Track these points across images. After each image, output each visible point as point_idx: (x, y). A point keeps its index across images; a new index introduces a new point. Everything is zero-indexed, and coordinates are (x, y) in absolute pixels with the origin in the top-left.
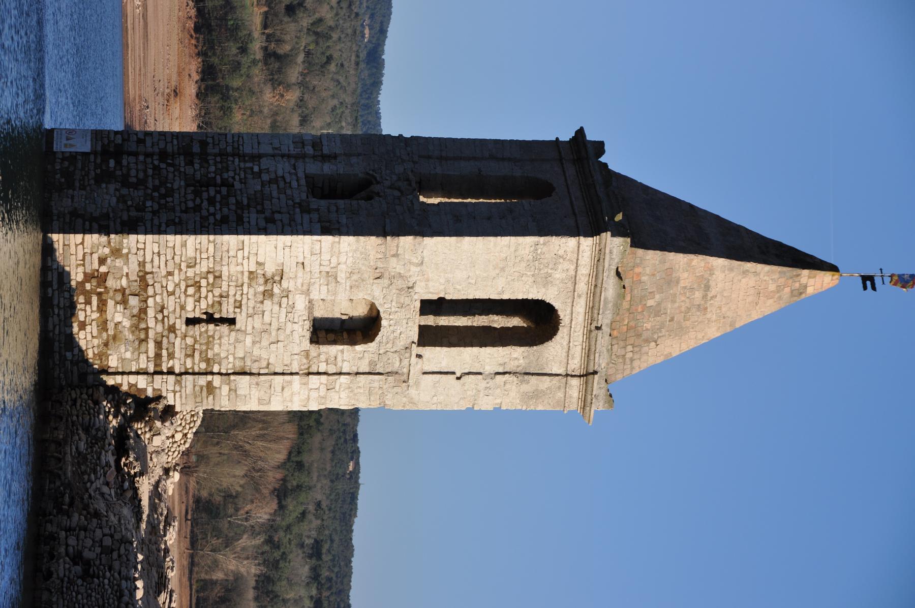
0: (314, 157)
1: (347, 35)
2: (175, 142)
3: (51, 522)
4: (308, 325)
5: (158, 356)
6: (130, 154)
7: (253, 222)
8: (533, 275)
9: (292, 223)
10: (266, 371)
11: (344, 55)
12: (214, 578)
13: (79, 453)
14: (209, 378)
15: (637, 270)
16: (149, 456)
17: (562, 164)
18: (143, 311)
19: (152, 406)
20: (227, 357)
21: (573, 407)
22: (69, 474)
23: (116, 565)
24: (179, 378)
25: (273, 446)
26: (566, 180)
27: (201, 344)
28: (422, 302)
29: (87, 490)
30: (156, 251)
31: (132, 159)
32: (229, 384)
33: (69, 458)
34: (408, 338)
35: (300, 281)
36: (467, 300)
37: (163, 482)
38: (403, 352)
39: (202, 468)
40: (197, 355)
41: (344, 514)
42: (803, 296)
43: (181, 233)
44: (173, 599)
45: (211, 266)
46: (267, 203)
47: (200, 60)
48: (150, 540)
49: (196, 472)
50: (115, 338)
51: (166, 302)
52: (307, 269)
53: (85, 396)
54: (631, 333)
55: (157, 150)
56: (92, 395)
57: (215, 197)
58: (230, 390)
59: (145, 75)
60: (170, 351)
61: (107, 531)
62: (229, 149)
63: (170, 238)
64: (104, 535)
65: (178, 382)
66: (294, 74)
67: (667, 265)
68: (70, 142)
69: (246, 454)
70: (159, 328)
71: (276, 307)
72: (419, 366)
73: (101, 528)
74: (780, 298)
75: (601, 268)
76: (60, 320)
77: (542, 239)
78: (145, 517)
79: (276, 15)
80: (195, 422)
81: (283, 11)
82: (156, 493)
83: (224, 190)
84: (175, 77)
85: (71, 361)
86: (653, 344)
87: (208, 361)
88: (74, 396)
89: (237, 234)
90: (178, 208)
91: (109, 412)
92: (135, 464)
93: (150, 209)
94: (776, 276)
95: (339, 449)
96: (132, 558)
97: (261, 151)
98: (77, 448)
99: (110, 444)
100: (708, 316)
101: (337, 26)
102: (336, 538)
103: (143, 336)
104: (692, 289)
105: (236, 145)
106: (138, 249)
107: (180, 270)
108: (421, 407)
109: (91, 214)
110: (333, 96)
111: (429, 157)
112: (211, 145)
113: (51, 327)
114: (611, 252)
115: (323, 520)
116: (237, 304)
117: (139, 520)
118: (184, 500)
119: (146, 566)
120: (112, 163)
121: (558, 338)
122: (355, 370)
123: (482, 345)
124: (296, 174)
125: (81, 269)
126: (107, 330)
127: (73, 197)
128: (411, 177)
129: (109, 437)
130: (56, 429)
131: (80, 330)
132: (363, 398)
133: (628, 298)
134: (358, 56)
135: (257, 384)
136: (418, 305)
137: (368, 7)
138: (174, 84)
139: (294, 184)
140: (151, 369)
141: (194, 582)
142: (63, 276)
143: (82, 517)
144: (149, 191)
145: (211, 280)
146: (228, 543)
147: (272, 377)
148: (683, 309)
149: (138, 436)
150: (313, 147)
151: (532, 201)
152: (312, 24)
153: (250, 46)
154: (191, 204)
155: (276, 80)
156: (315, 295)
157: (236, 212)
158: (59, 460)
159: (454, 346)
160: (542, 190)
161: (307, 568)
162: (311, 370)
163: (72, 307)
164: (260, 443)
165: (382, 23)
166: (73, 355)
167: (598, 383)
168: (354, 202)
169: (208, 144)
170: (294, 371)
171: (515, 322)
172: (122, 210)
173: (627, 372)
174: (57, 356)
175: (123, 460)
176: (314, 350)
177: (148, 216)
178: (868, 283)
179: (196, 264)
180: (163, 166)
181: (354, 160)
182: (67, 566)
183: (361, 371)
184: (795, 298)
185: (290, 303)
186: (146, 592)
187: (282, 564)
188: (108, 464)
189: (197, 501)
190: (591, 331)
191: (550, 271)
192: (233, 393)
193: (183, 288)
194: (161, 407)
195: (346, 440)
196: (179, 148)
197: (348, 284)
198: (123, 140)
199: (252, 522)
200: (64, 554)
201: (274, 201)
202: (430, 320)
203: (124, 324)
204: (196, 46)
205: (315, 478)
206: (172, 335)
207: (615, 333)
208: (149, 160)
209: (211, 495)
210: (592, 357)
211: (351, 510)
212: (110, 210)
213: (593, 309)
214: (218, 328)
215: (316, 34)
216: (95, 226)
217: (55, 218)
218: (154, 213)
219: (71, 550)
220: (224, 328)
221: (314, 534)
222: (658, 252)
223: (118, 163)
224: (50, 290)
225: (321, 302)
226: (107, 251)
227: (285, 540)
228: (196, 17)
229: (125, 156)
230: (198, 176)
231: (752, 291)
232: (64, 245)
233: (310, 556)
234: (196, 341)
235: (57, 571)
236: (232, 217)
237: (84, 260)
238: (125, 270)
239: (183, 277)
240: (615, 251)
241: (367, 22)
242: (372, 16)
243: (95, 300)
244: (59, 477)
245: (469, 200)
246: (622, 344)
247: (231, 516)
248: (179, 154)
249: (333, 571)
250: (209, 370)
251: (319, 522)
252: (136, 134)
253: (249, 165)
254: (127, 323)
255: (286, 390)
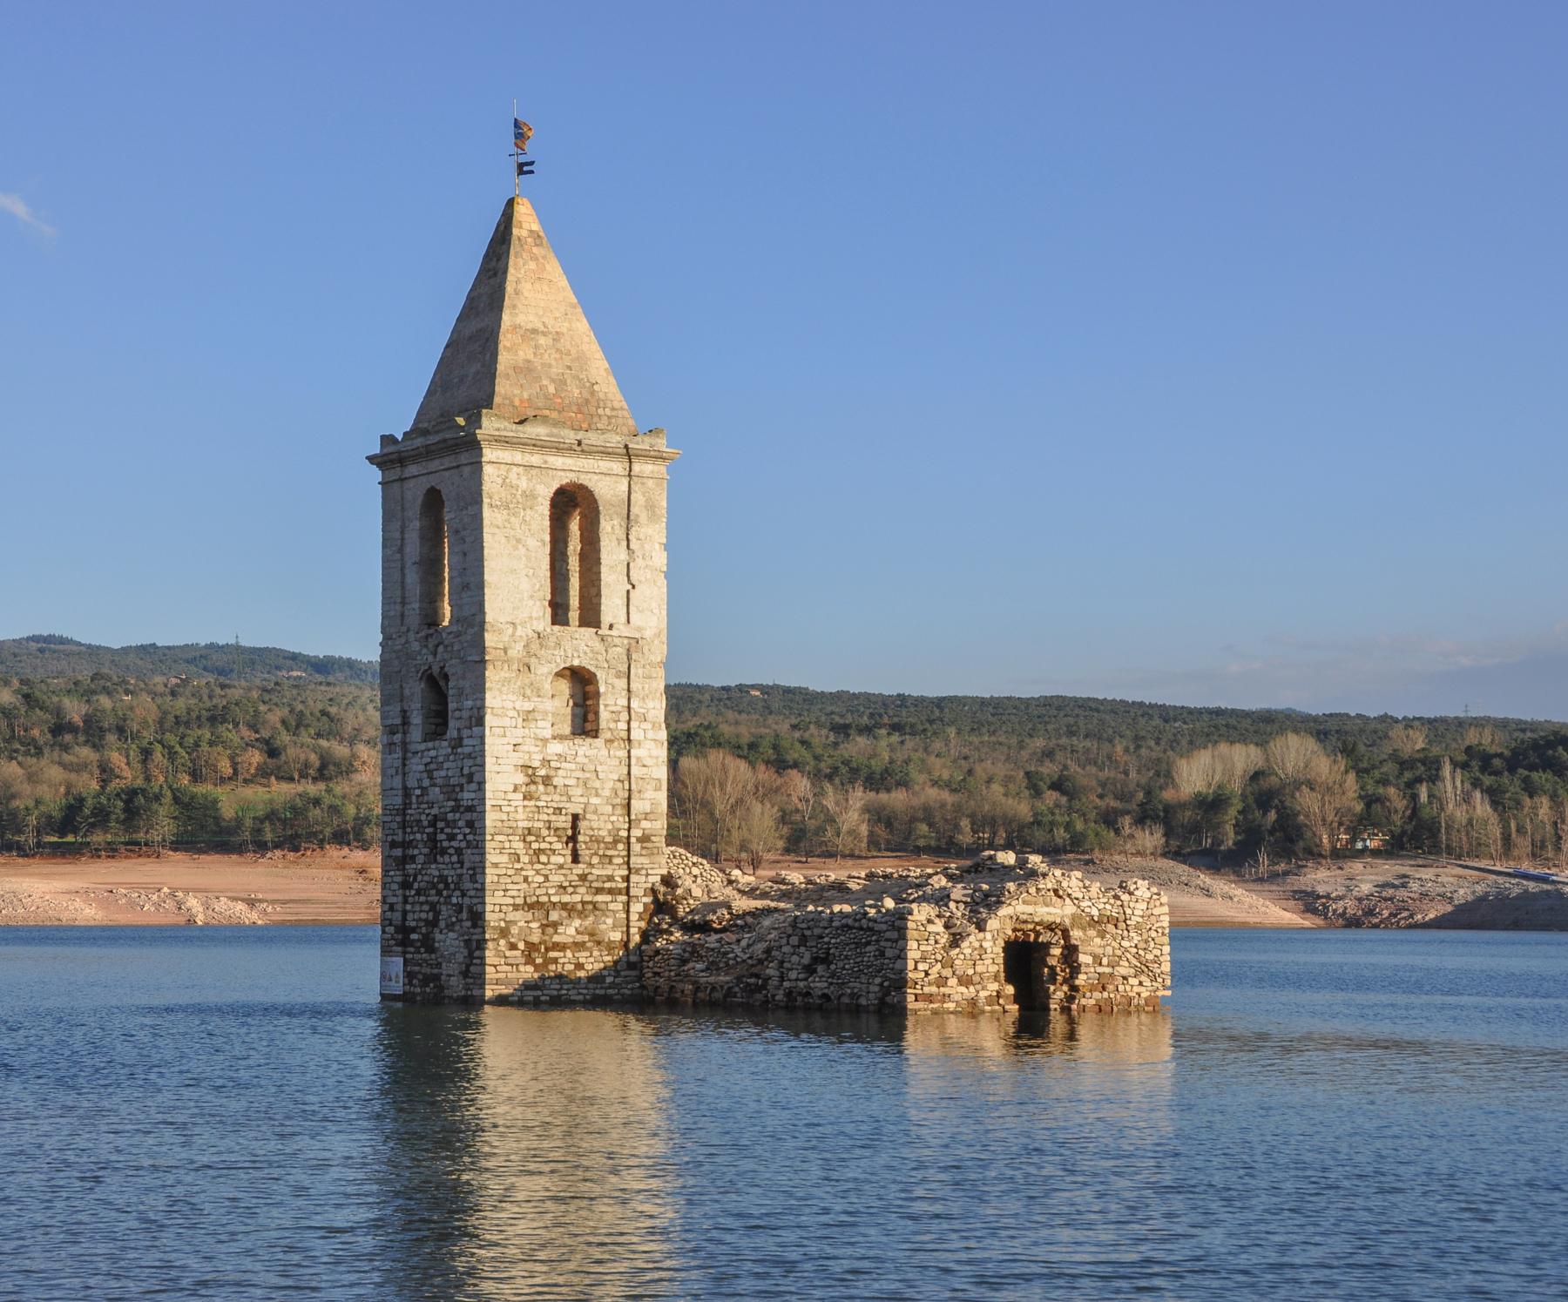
0: (404, 733)
1: (298, 694)
2: (392, 873)
3: (773, 996)
4: (578, 741)
5: (610, 891)
6: (404, 919)
7: (472, 795)
8: (524, 510)
9: (473, 755)
10: (626, 783)
11: (320, 698)
12: (866, 833)
13: (707, 969)
14: (633, 840)
15: (517, 403)
16: (712, 900)
17: (406, 478)
18: (564, 906)
19: (661, 897)
20: (613, 822)
21: (663, 469)
22: (728, 978)
23: (817, 931)
24: (633, 871)
25: (732, 772)
26: (423, 475)
27: (599, 849)
28: (554, 623)
29: (744, 961)
30: (502, 893)
31: (410, 916)
32: (640, 821)
33: (712, 979)
34: (592, 639)
35: (533, 749)
36: (551, 577)
37: (740, 886)
38: (606, 644)
39: (754, 847)
40: (609, 853)
41: (804, 700)
42: (541, 234)
43: (484, 868)
44: (857, 875)
45: (518, 838)
46: (452, 781)
47: (328, 847)
48: (797, 898)
49: (757, 853)
50: (592, 935)
51: (555, 884)
52: (520, 741)
53: (651, 964)
54: (585, 409)
55: (400, 891)
56: (650, 957)
57: (447, 834)
58: (645, 819)
59: (345, 903)
60: (605, 879)
61: (784, 941)
62: (399, 819)
63: (488, 879)
64: (788, 944)
65: (638, 871)
66: (340, 750)
67: (511, 372)
68: (393, 977)
69: (740, 802)
70: (582, 890)
71: (560, 772)
72: (621, 627)
73: (781, 947)
74: (544, 257)
75: (515, 440)
76: (574, 988)
77: (486, 500)
78: (773, 904)
79: (279, 768)
80: (680, 855)
81: (275, 760)
82: (751, 893)
83: (440, 825)
84: (346, 873)
85: (615, 977)
86: (595, 387)
87: (616, 842)
88: (650, 975)
89: (485, 811)
90: (459, 871)
91: (667, 940)
92: (719, 914)
93: (460, 899)
94: (521, 262)
95: (737, 705)
96: (811, 916)
97: (400, 786)
98: (702, 971)
99: (699, 939)
100: (565, 330)
101: (290, 705)
102: (829, 709)
103: (590, 907)
104: (536, 347)
105: (395, 812)
106: (500, 911)
107: (522, 869)
108: (664, 625)
109: (465, 957)
110: (364, 710)
111: (402, 615)
112: (395, 837)
113: (581, 998)
114: (498, 430)
115: (810, 723)
116: (558, 812)
117: (776, 910)
118: (786, 864)
119: (822, 902)
120: (414, 936)
121: (590, 485)
122: (625, 693)
123: (598, 562)
124: (423, 751)
125: (522, 968)
126: (584, 942)
127: (449, 976)
128: (423, 634)
129: (691, 940)
130: (683, 991)
131: (583, 969)
132: (655, 685)
133: (547, 412)
134: (321, 683)
135: (640, 792)
136: (556, 628)
137: (269, 673)
138: (353, 874)
139: (433, 753)
140: (624, 898)
141: (870, 854)
142: (528, 986)
143: (771, 965)
144: (442, 899)
145: (533, 838)
146: (831, 820)
147: (632, 777)
148: (558, 356)
149: (692, 911)
150: (394, 734)
151: (445, 510)
152: (288, 731)
153: (312, 795)
154: (455, 859)
155: (347, 769)
156: (548, 733)
157: (462, 813)
158: (714, 988)
159: (599, 591)
160: (433, 501)
161: (859, 739)
162: (626, 737)
163: (560, 977)
164: (729, 789)
165: (285, 658)
166: (609, 975)
167: (638, 444)
168: (451, 692)
169: (393, 840)
170: (626, 755)
171: (574, 526)
172: (461, 927)
173: (626, 414)
174: (611, 991)
175: (715, 925)
176: (606, 735)
177: (467, 901)
178: (525, 169)
179: (515, 854)
180: (416, 885)
181: (407, 692)
182: (817, 979)
183: (626, 687)
184: (545, 241)
185: (556, 758)
186: (847, 902)
187: (854, 765)
188: (719, 941)
189: (787, 851)
190: (582, 451)
191: (520, 493)
192: (649, 817)
193: (541, 866)
194: (662, 889)
195: (728, 699)
196: (398, 870)
197: (536, 699)
198: (390, 925)
199: (810, 796)
200: (806, 983)
201: (450, 774)
202: (574, 615)
203: (577, 925)
204: (314, 850)
205: (767, 731)
206: (590, 877)
207: (585, 426)
208: (410, 899)
209: (781, 837)
210: (610, 450)
211: (800, 693)
212: (461, 938)
213: (559, 448)
214: (582, 831)
215: (297, 727)
216: (477, 953)
217: (469, 993)
218: (463, 895)
219: (801, 976)
220: (582, 825)
221: (824, 732)
222: (497, 381)
223: (414, 930)
224: (543, 998)
225: (555, 727)
226: (502, 942)
227: (830, 761)
228: (283, 850)
229: (407, 923)
230: (426, 851)
231: (537, 285)
232: (497, 984)
233: (847, 735)
234: (596, 854)
235: (822, 989)
236: (468, 816)
237: (512, 965)
238: (522, 924)
239: (529, 866)
240: (497, 425)
241: (284, 673)
242: (278, 668)
243: (552, 954)
244: (729, 988)
245: (446, 575)
246: (595, 419)
247: (804, 817)
248: (404, 869)
249: (863, 712)
250: (625, 841)
251: (812, 726)
252: (385, 912)
253: (414, 799)
254: (577, 923)
255: (646, 763)
